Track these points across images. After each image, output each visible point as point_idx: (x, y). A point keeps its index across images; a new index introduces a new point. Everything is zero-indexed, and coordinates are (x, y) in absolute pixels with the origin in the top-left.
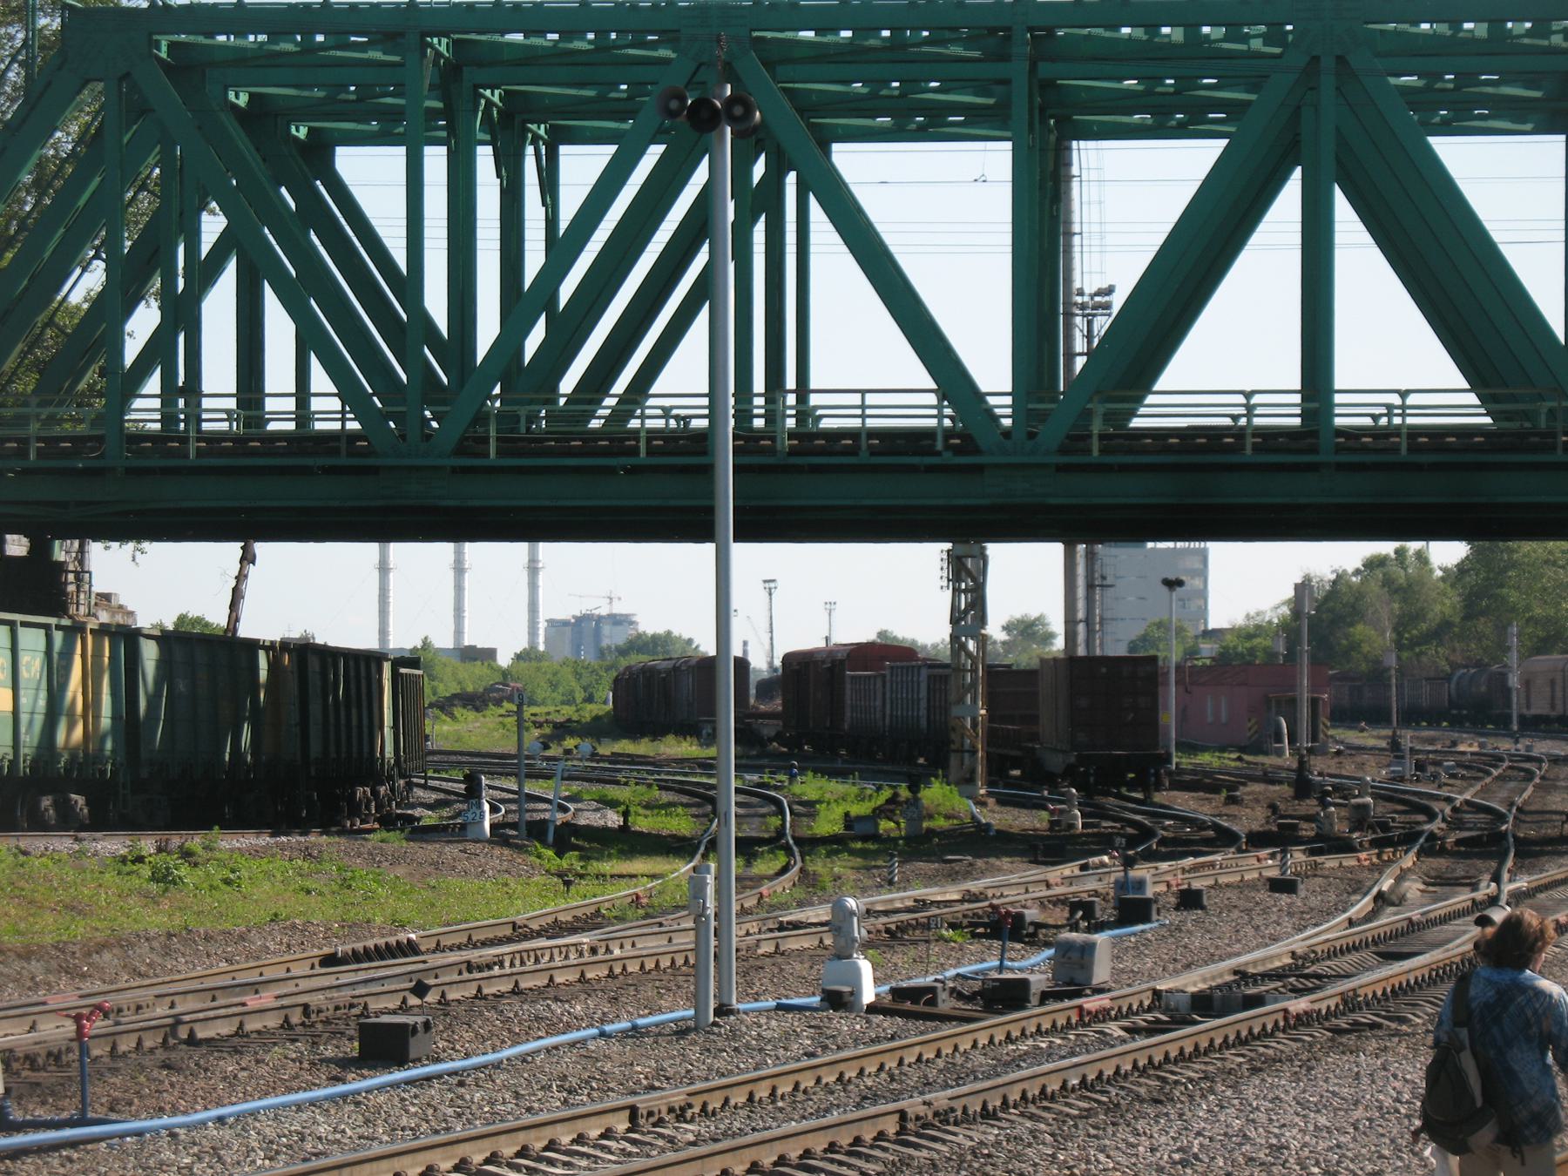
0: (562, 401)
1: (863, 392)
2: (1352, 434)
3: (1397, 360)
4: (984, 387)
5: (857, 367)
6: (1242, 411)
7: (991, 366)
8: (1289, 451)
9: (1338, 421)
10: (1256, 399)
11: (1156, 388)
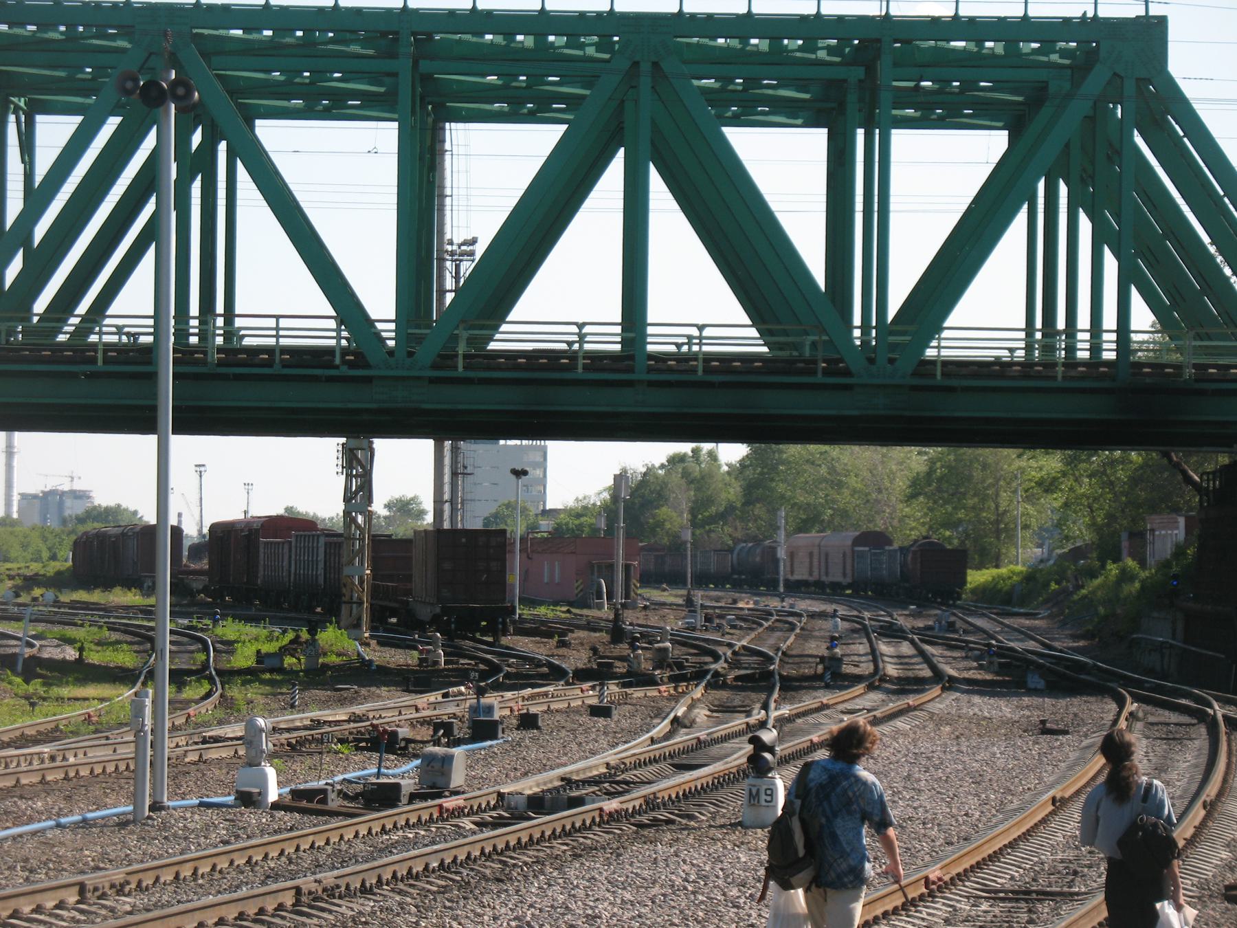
0: (35, 319)
1: (278, 317)
3: (696, 303)
5: (273, 297)
6: (576, 338)
7: (380, 299)
9: (650, 348)
11: (109, 312)
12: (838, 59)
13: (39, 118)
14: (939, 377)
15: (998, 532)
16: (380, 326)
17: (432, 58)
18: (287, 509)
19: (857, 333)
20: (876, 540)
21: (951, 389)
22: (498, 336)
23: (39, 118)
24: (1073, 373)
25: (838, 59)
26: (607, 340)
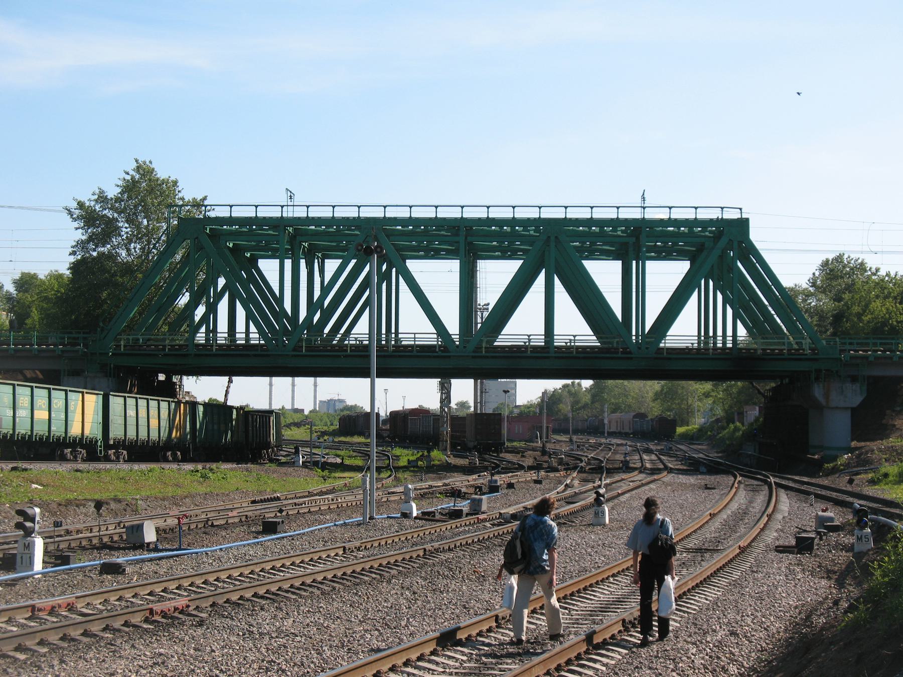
5: (413, 326)
7: (453, 327)
10: (577, 338)
15: (688, 413)
20: (642, 416)
21: (670, 359)
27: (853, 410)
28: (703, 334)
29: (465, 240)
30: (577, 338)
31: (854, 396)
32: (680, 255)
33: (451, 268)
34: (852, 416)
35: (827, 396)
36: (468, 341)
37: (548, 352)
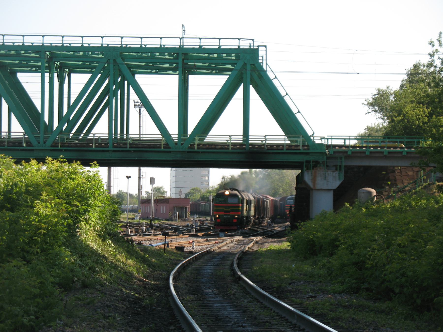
0: (188, 136)
1: (350, 136)
2: (254, 145)
3: (266, 129)
4: (171, 133)
5: (141, 127)
6: (229, 139)
7: (173, 129)
8: (74, 147)
9: (250, 142)
10: (232, 137)
11: (209, 134)
12: (172, 58)
13: (191, 77)
14: (196, 149)
16: (172, 136)
17: (188, 60)
18: (119, 191)
19: (125, 136)
21: (199, 152)
22: (206, 139)
23: (191, 77)
24: (235, 148)
25: (172, 58)
26: (239, 140)
27: (334, 191)
28: (119, 132)
29: (184, 62)
30: (267, 137)
31: (334, 181)
32: (220, 72)
33: (171, 81)
34: (334, 195)
35: (314, 180)
36: (184, 140)
37: (108, 147)
